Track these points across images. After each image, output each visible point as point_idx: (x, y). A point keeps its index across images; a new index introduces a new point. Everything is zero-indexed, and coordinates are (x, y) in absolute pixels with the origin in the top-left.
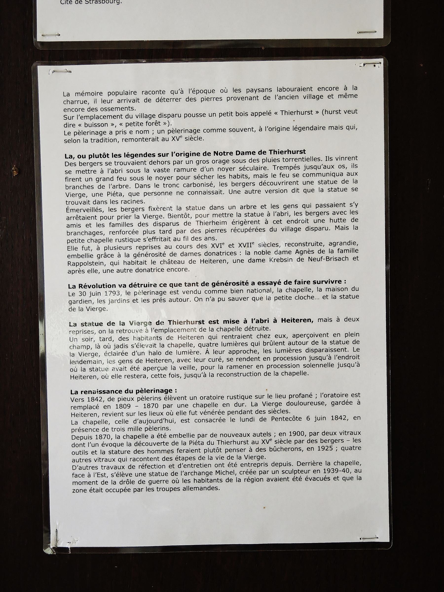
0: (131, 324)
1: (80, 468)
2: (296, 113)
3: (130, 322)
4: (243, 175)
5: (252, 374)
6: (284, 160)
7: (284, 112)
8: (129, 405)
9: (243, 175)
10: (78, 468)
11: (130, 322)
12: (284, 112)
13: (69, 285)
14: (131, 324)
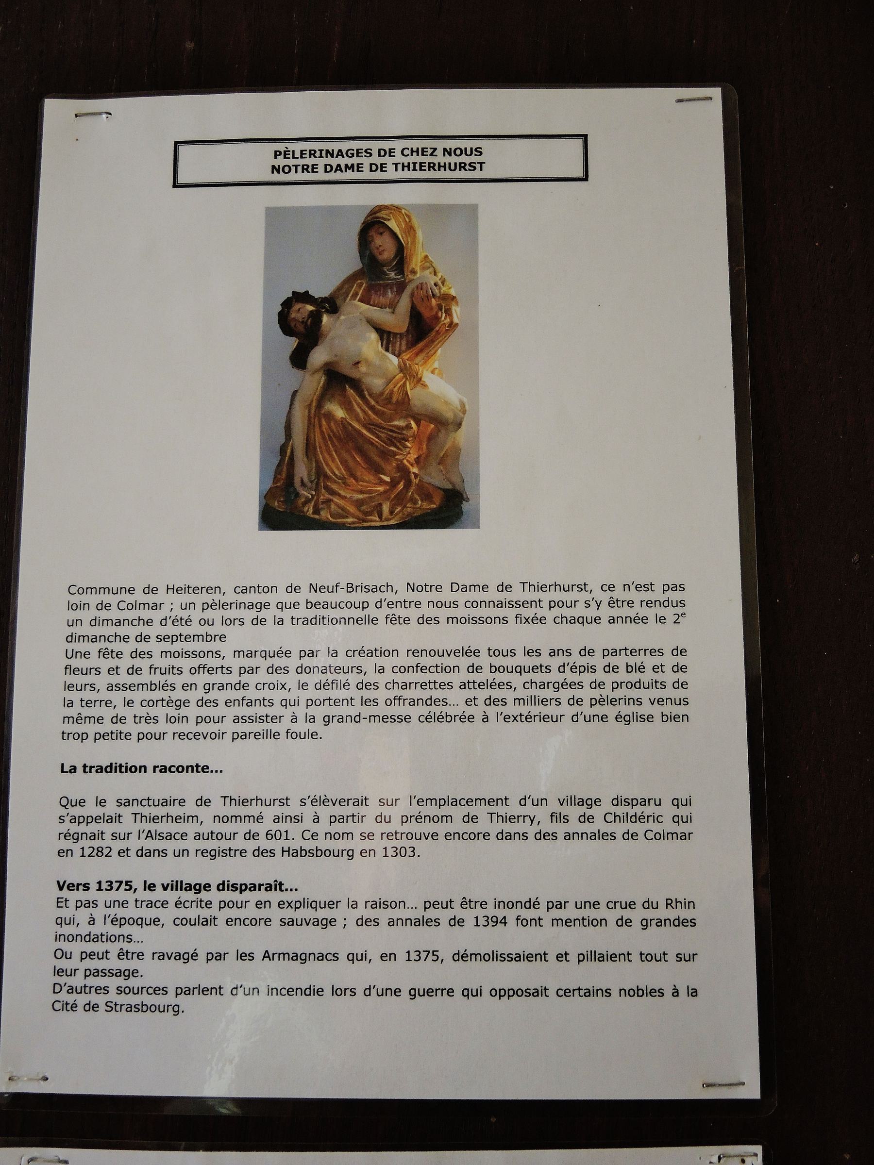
0: (61, 888)
1: (71, 990)
2: (165, 819)
3: (58, 882)
4: (173, 668)
5: (439, 669)
6: (492, 653)
7: (527, 585)
8: (269, 837)
9: (173, 668)
10: (65, 989)
11: (58, 882)
12: (527, 585)
13: (63, 765)
14: (61, 888)
